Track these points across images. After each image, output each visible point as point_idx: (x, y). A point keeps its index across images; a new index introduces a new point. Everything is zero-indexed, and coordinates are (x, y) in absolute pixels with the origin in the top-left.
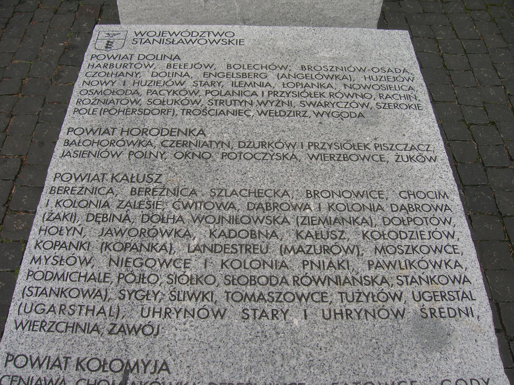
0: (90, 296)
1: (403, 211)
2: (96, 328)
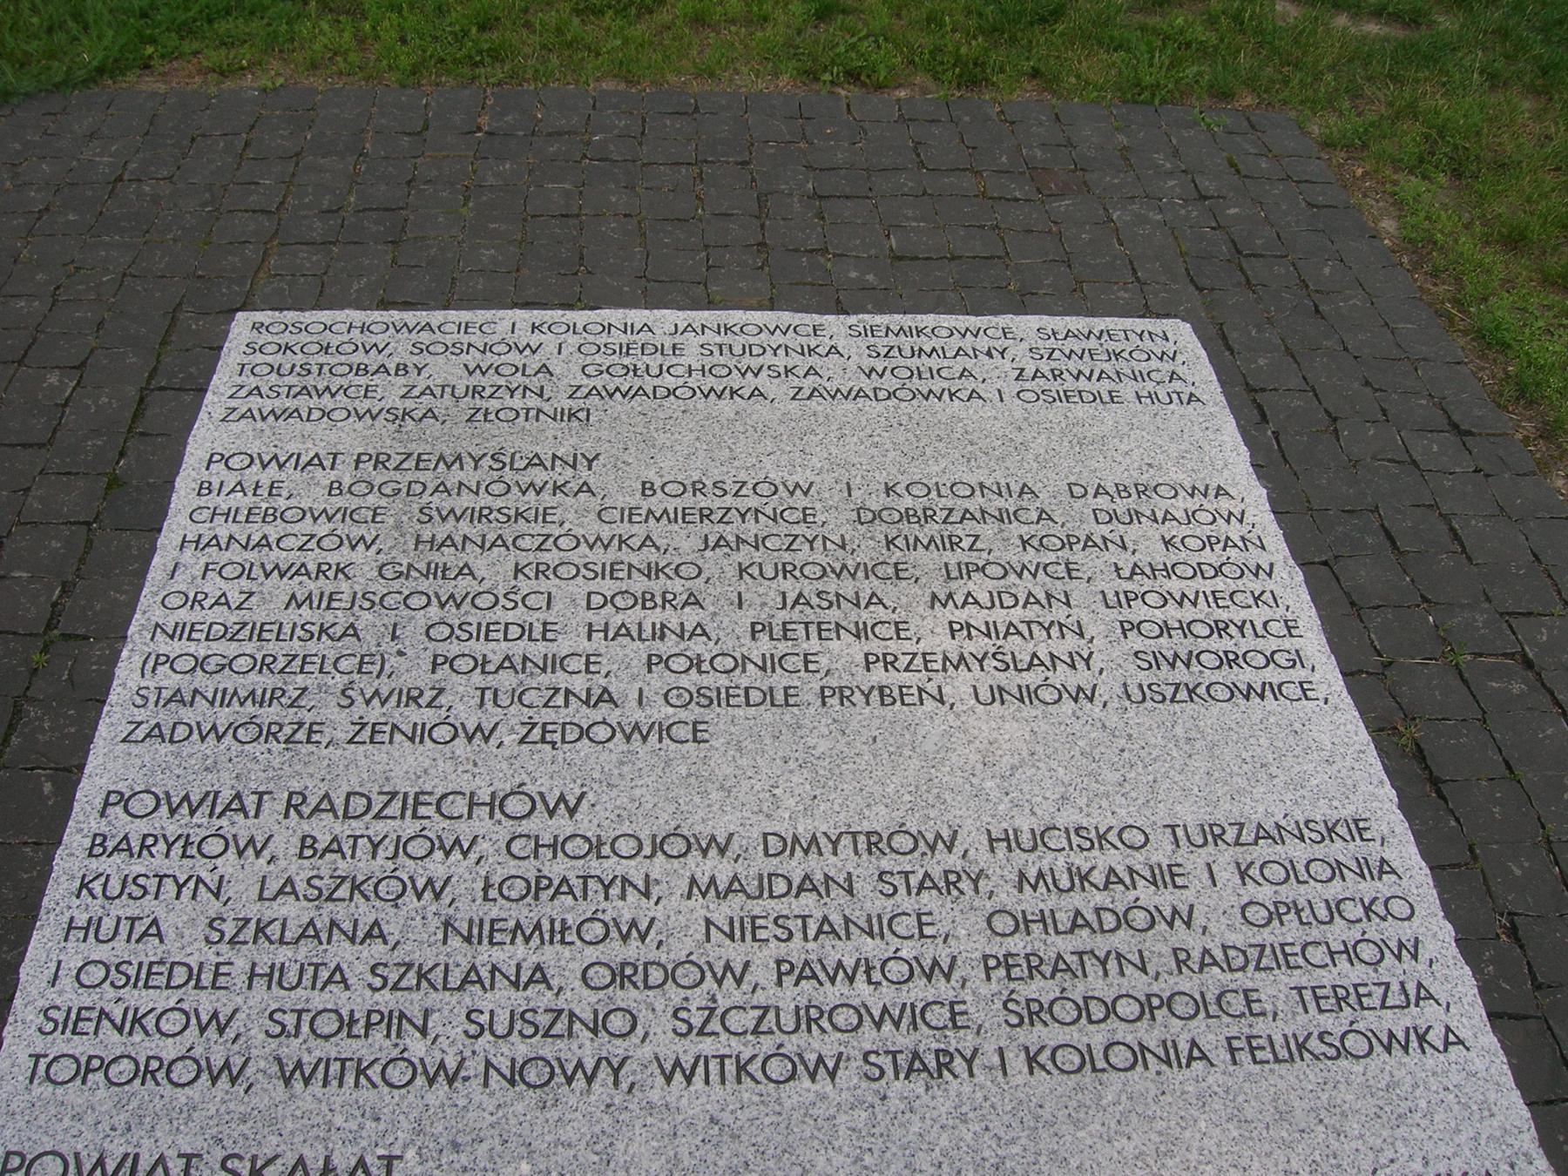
2: (1197, 1053)
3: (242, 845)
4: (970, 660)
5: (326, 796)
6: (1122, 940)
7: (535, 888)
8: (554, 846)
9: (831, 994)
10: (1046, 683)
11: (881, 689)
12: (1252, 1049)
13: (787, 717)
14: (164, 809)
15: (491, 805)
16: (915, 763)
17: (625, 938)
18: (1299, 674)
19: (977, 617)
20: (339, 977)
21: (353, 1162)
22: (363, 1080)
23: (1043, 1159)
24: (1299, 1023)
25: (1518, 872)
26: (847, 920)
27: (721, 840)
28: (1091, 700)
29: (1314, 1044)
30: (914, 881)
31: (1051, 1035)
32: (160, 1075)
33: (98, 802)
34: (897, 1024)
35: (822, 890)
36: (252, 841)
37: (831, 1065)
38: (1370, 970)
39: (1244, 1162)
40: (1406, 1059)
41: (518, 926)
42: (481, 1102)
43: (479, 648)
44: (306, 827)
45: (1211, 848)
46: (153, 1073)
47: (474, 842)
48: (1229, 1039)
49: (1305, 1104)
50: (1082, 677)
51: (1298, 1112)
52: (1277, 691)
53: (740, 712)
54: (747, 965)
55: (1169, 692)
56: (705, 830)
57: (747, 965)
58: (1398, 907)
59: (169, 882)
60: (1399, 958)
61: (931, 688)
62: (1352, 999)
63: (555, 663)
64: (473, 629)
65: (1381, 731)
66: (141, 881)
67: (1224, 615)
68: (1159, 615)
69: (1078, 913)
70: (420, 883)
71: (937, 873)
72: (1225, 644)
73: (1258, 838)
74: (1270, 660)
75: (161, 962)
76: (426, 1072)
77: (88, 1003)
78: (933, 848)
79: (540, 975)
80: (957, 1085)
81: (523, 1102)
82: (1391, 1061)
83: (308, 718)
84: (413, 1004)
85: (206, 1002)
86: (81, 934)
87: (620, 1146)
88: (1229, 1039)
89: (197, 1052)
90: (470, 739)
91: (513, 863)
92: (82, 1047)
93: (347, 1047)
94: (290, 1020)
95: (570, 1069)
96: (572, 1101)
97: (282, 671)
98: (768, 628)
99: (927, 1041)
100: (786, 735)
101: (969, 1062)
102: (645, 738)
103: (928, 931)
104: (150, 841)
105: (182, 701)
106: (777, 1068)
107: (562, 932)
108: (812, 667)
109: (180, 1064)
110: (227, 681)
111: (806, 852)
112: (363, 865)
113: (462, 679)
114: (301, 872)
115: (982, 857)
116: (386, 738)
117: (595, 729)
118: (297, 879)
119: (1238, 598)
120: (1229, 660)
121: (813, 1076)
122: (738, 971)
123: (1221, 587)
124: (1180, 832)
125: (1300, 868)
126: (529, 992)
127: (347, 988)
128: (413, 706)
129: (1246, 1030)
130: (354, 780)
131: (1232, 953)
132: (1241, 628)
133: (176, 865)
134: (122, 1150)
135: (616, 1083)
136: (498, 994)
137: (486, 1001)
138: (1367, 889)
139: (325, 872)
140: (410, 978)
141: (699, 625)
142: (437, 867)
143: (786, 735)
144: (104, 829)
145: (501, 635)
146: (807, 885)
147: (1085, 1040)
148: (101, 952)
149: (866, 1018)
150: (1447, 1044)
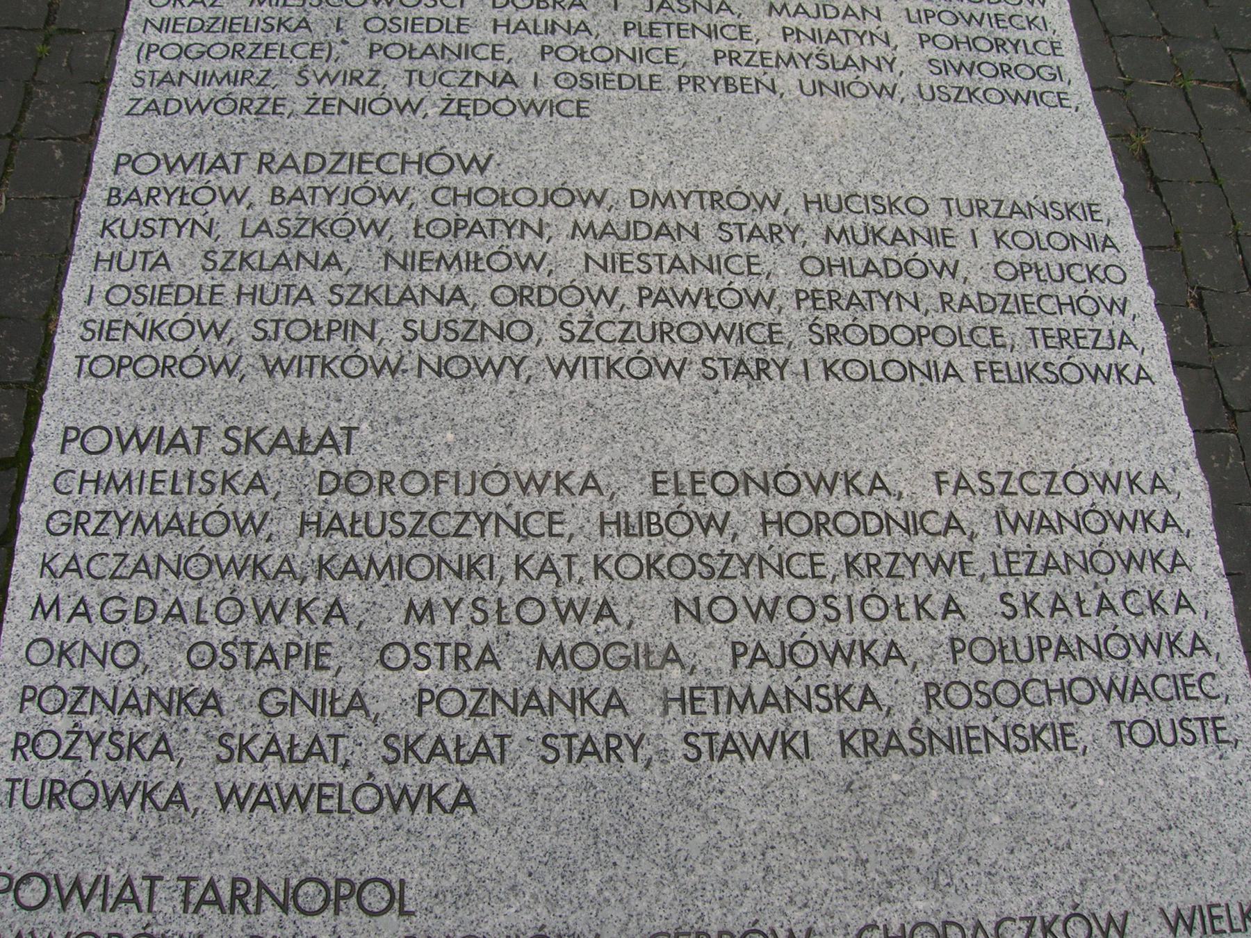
0: (242, 806)
2: (952, 372)
3: (226, 194)
4: (798, 59)
5: (290, 156)
6: (902, 284)
7: (455, 228)
8: (468, 196)
9: (680, 314)
10: (857, 81)
11: (726, 79)
12: (993, 371)
13: (651, 99)
14: (164, 167)
15: (419, 163)
16: (751, 139)
17: (524, 267)
18: (1058, 86)
19: (806, 25)
20: (306, 295)
21: (322, 432)
22: (327, 372)
23: (831, 442)
24: (1030, 355)
25: (1210, 257)
26: (693, 259)
27: (598, 194)
28: (892, 96)
30: (746, 231)
32: (175, 370)
33: (112, 163)
34: (728, 339)
35: (675, 235)
36: (233, 192)
37: (678, 367)
38: (1088, 319)
39: (980, 453)
40: (1107, 387)
41: (442, 257)
42: (418, 389)
43: (407, 38)
44: (275, 180)
45: (975, 218)
46: (169, 368)
47: (406, 192)
48: (976, 363)
49: (1028, 414)
50: (886, 77)
51: (1023, 420)
52: (1039, 98)
53: (614, 94)
54: (616, 290)
55: (953, 93)
56: (586, 186)
57: (616, 290)
58: (1114, 274)
59: (171, 224)
60: (1110, 311)
61: (766, 80)
62: (1072, 340)
63: (468, 51)
64: (402, 23)
65: (1116, 136)
66: (150, 223)
67: (1003, 35)
68: (950, 31)
69: (870, 261)
70: (366, 224)
71: (763, 225)
72: (1002, 58)
73: (1012, 212)
74: (1036, 73)
75: (170, 285)
76: (374, 366)
77: (116, 317)
78: (761, 206)
79: (459, 294)
80: (771, 386)
81: (447, 389)
82: (1096, 388)
83: (273, 94)
84: (363, 315)
85: (206, 315)
86: (107, 265)
87: (520, 421)
88: (976, 363)
89: (202, 352)
90: (401, 111)
91: (437, 208)
92: (115, 350)
93: (316, 348)
94: (270, 327)
95: (482, 364)
96: (485, 388)
97: (250, 57)
98: (638, 26)
99: (751, 353)
100: (650, 114)
101: (781, 369)
102: (539, 113)
103: (755, 269)
104: (154, 192)
105: (172, 82)
106: (637, 368)
107: (476, 263)
108: (672, 59)
109: (189, 362)
110: (207, 65)
111: (664, 205)
112: (322, 210)
113: (394, 63)
114: (273, 215)
115: (799, 215)
116: (335, 110)
117: (500, 104)
118: (270, 221)
119: (1015, 21)
120: (1003, 71)
122: (610, 294)
123: (1002, 11)
124: (953, 204)
125: (1043, 238)
126: (451, 307)
127: (313, 303)
128: (356, 85)
129: (990, 357)
130: (312, 144)
131: (984, 299)
132: (1015, 46)
133: (175, 211)
134: (151, 424)
135: (517, 376)
136: (427, 308)
137: (419, 314)
138: (1092, 258)
139: (291, 215)
140: (361, 297)
141: (582, 22)
142: (378, 211)
143: (650, 114)
144: (118, 184)
145: (424, 28)
146: (663, 231)
147: (869, 357)
148: (123, 279)
149: (705, 333)
150: (1138, 378)
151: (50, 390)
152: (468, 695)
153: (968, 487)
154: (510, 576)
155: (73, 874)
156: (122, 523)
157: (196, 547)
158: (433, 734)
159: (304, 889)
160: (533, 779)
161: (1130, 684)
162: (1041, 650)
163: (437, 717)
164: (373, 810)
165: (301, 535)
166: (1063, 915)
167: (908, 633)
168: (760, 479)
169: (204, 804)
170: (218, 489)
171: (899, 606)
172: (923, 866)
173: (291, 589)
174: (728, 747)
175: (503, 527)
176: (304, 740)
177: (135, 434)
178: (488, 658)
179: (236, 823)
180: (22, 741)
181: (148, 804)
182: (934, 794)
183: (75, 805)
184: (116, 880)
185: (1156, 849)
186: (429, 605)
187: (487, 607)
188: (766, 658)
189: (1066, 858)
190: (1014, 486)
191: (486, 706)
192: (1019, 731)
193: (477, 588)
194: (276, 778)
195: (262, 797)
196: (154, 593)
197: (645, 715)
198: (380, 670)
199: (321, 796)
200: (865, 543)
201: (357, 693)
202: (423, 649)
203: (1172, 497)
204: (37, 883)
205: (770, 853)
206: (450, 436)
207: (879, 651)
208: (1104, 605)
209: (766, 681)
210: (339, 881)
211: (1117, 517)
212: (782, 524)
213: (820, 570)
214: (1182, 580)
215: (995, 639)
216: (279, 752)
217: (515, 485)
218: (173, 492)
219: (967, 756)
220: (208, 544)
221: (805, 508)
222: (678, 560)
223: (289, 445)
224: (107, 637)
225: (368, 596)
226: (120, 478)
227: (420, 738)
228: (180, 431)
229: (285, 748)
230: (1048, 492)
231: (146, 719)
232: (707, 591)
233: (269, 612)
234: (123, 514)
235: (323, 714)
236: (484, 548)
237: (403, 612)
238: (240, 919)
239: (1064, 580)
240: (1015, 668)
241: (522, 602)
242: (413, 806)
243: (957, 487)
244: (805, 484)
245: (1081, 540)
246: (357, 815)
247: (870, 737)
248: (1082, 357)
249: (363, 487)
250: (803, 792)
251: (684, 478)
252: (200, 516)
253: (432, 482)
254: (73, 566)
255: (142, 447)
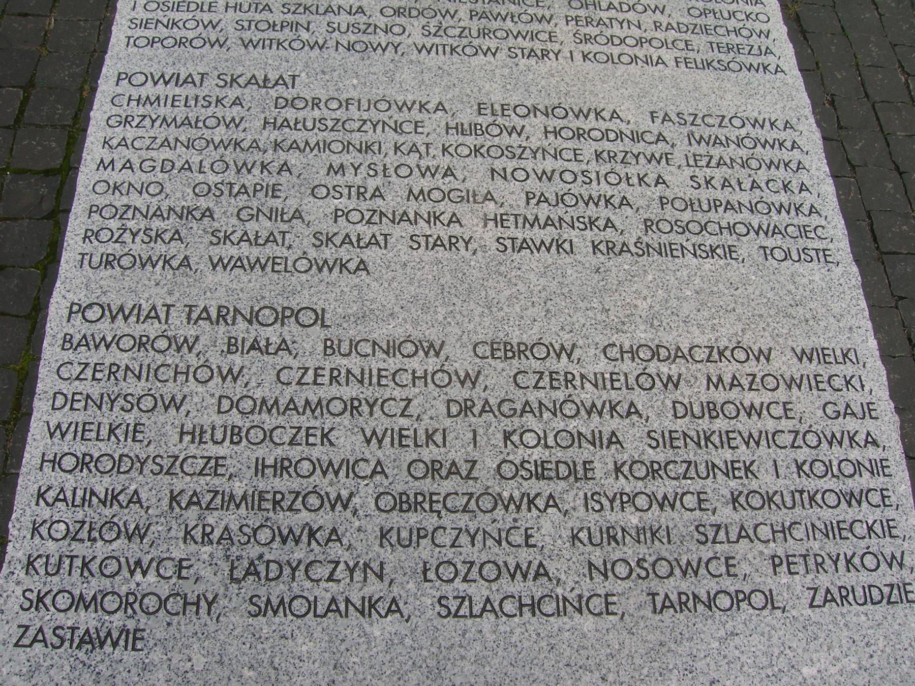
0: (225, 268)
1: (613, 447)
2: (660, 61)
9: (495, 25)
24: (710, 56)
29: (715, 64)
31: (595, 48)
34: (524, 38)
42: (335, 57)
54: (456, 11)
57: (456, 11)
80: (550, 64)
81: (354, 57)
84: (303, 19)
85: (206, 17)
87: (398, 75)
89: (203, 36)
92: (150, 34)
94: (246, 24)
96: (376, 58)
99: (538, 46)
101: (557, 55)
121: (485, 55)
135: (396, 52)
137: (336, 19)
140: (301, 10)
150: (776, 71)
151: (109, 53)
152: (365, 213)
153: (670, 120)
154: (392, 153)
155: (119, 303)
156: (153, 121)
157: (200, 134)
158: (344, 233)
159: (263, 312)
160: (404, 258)
161: (771, 228)
162: (716, 206)
163: (345, 224)
164: (306, 271)
165: (264, 128)
166: (731, 347)
167: (634, 193)
168: (543, 110)
169: (202, 267)
170: (213, 105)
171: (628, 179)
172: (644, 315)
173: (258, 156)
174: (525, 245)
175: (387, 128)
176: (264, 234)
177: (162, 76)
178: (378, 193)
179: (221, 276)
180: (89, 234)
181: (167, 266)
182: (650, 277)
183: (121, 267)
184: (146, 307)
185: (788, 316)
186: (342, 166)
187: (377, 168)
188: (546, 201)
189: (732, 316)
190: (699, 121)
191: (376, 218)
192: (703, 247)
193: (369, 158)
194: (247, 254)
195: (239, 263)
196: (174, 158)
197: (471, 223)
198: (311, 199)
199: (274, 263)
200: (607, 145)
201: (297, 210)
202: (337, 189)
203: (798, 133)
204: (96, 308)
205: (549, 303)
206: (355, 81)
207: (616, 201)
208: (754, 185)
209: (546, 213)
210: (284, 309)
211: (763, 141)
212: (556, 133)
213: (580, 158)
214: (804, 176)
215: (687, 199)
216: (249, 240)
217: (394, 107)
218: (185, 106)
219: (670, 258)
220: (207, 134)
221: (570, 126)
222: (493, 149)
223: (257, 83)
224: (144, 179)
225: (305, 161)
226: (153, 99)
227: (335, 234)
228: (190, 75)
229: (252, 238)
230: (720, 126)
231: (167, 222)
232: (511, 165)
233: (244, 168)
234: (154, 117)
235: (276, 220)
236: (375, 138)
237: (326, 169)
238: (222, 328)
239: (730, 171)
240: (700, 215)
241: (398, 166)
242: (331, 270)
243: (664, 120)
244: (571, 114)
245: (740, 152)
246: (296, 274)
247: (610, 245)
248: (741, 58)
249: (302, 105)
250: (569, 272)
251: (497, 107)
252: (201, 118)
253: (344, 104)
254: (123, 143)
255: (166, 83)
